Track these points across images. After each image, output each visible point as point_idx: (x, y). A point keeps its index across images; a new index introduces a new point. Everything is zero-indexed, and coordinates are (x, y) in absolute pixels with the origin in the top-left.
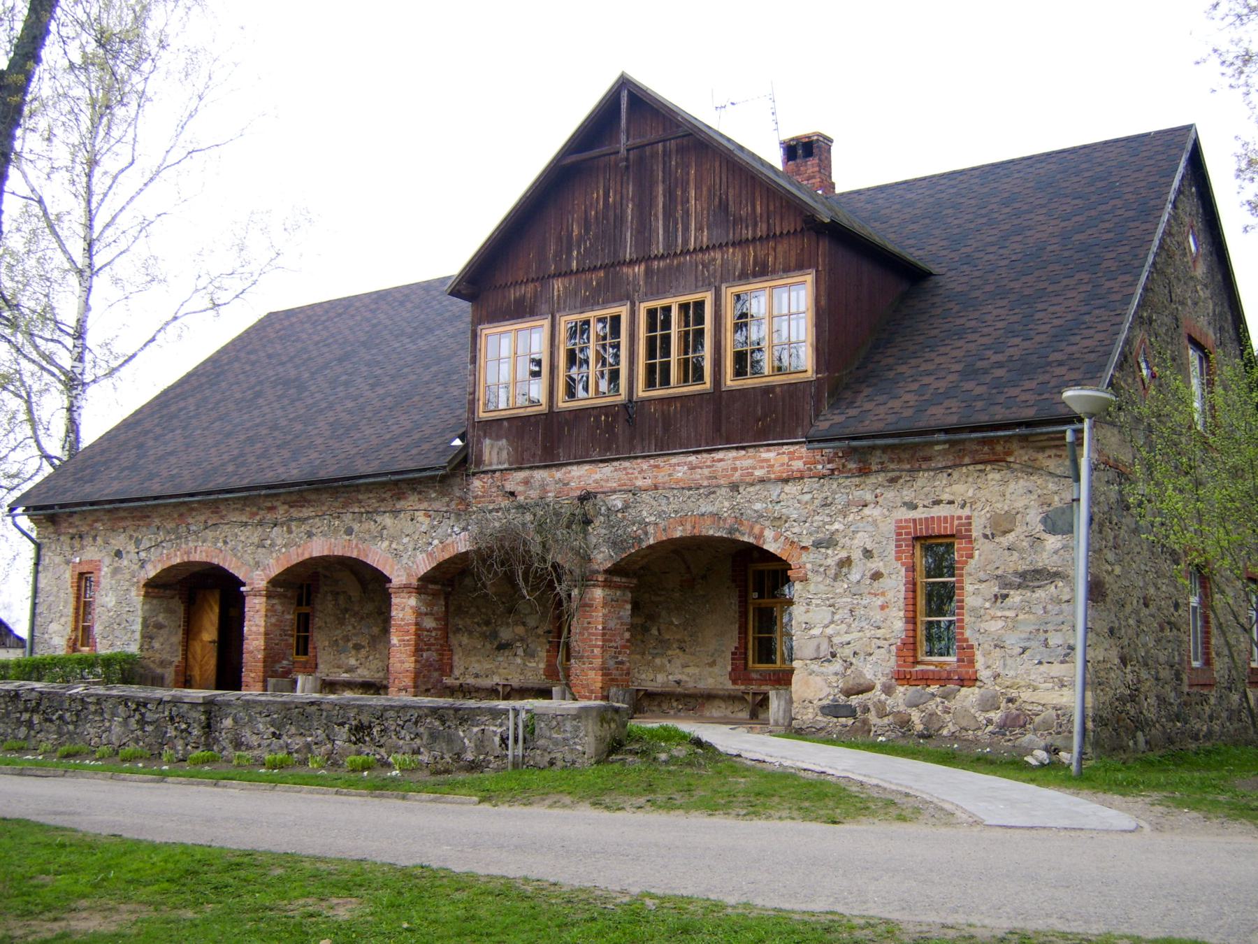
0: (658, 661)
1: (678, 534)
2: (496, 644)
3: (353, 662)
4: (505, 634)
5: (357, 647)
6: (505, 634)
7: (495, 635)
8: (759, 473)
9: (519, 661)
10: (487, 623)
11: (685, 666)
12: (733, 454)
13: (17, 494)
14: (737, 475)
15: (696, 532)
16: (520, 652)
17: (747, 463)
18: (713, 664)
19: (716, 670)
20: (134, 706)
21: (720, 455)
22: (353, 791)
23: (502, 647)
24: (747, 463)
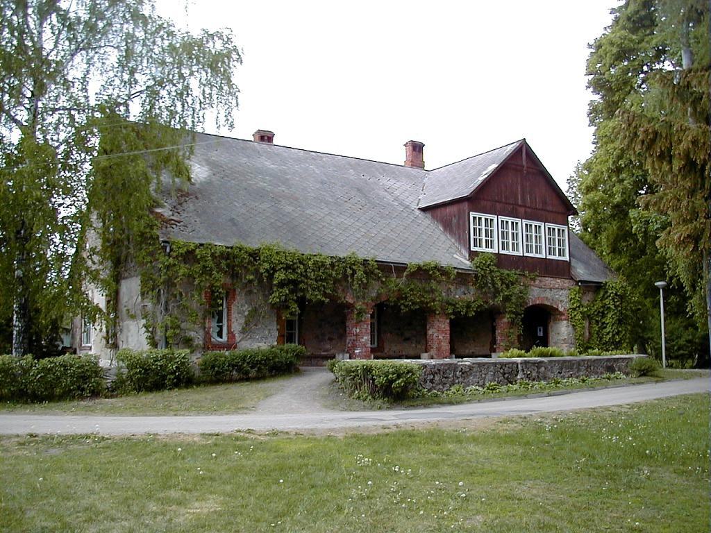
0: (466, 345)
1: (538, 302)
2: (403, 338)
3: (328, 346)
4: (407, 334)
5: (331, 339)
6: (407, 334)
7: (402, 334)
8: (557, 286)
9: (414, 345)
10: (399, 329)
11: (475, 346)
12: (550, 279)
13: (657, 110)
14: (551, 286)
15: (534, 303)
16: (414, 342)
17: (554, 282)
18: (483, 346)
19: (485, 348)
20: (500, 366)
21: (547, 279)
22: (148, 414)
23: (407, 339)
24: (554, 282)
